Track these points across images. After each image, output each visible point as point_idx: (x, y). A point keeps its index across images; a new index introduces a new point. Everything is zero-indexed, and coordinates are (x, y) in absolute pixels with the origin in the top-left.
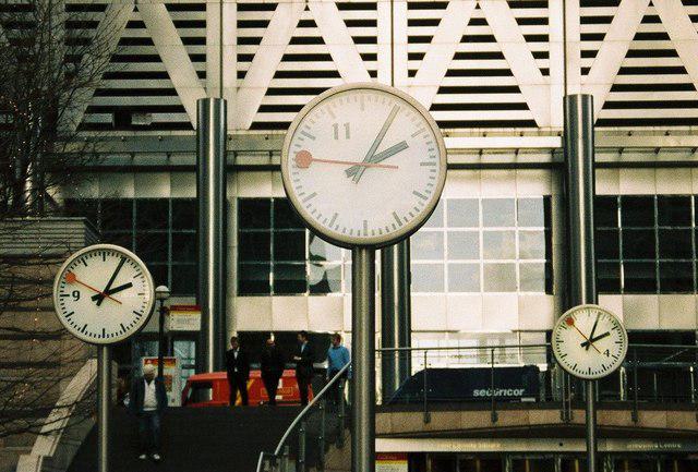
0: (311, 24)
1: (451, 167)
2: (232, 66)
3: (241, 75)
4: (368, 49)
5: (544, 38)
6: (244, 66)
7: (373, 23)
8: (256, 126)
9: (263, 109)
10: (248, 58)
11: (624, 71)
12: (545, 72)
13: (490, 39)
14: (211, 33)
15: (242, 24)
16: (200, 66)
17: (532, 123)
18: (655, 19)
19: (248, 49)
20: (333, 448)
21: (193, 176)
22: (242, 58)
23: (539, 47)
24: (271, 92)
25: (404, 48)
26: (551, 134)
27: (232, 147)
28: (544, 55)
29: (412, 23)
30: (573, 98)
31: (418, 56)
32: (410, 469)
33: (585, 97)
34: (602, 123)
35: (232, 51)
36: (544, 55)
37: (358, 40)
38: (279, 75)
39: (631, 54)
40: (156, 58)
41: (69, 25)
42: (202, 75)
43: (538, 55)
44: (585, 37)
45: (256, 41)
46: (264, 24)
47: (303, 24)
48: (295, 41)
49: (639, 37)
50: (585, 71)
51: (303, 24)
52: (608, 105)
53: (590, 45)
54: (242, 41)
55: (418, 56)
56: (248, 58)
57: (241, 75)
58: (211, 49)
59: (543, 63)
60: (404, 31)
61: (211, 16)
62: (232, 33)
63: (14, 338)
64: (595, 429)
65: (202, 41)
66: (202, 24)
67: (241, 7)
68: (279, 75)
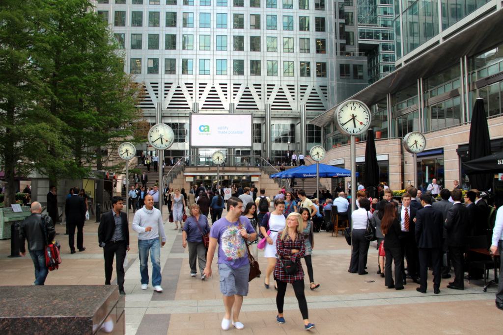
0: (214, 88)
1: (254, 117)
2: (163, 96)
3: (165, 97)
4: (156, 92)
5: (226, 91)
7: (226, 88)
8: (168, 108)
9: (170, 104)
10: (167, 94)
11: (242, 98)
12: (294, 99)
13: (283, 92)
14: (159, 89)
16: (157, 95)
17: (223, 108)
18: (248, 88)
19: (166, 92)
20: (179, 174)
21: (189, 118)
22: (165, 94)
23: (225, 93)
24: (171, 101)
25: (198, 93)
26: (261, 111)
27: (163, 112)
28: (226, 95)
29: (200, 87)
30: (231, 104)
31: (235, 95)
32: (502, 173)
33: (233, 104)
34: (237, 108)
35: (164, 92)
36: (226, 95)
37: (189, 91)
38: (173, 97)
39: (243, 95)
42: (157, 97)
43: (225, 95)
44: (234, 91)
46: (170, 87)
47: (212, 88)
48: (176, 91)
50: (234, 98)
51: (212, 88)
52: (238, 105)
53: (302, 94)
54: (268, 92)
55: (235, 95)
56: (167, 94)
57: (165, 97)
58: (159, 92)
59: (260, 97)
60: (198, 89)
65: (157, 90)
68: (173, 97)
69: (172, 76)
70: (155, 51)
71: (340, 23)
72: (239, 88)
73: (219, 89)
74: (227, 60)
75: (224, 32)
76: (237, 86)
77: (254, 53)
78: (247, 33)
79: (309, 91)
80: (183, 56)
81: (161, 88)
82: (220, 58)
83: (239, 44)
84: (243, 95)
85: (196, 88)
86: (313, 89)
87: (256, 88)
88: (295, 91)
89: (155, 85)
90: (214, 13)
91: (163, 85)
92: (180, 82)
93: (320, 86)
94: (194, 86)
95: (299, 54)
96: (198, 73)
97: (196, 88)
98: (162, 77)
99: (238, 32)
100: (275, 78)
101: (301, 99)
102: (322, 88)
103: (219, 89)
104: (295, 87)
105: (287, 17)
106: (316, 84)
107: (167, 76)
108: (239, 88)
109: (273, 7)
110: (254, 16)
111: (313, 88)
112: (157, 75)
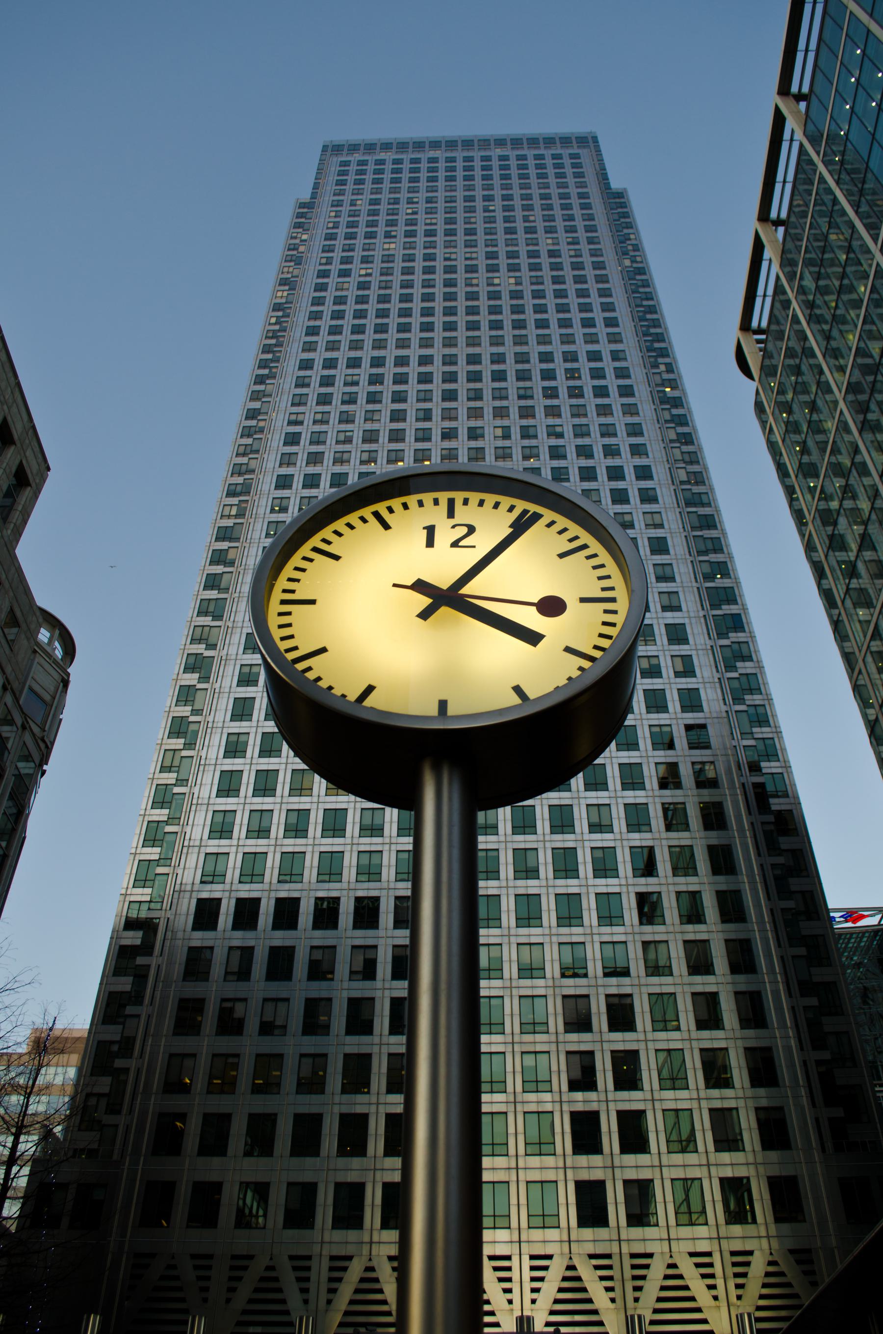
2: (324, 1296)
3: (329, 1302)
4: (507, 1285)
6: (637, 1294)
11: (556, 1301)
14: (313, 1275)
15: (532, 1268)
16: (305, 1296)
19: (639, 1283)
35: (324, 1287)
37: (501, 1280)
40: (280, 1290)
41: (196, 1267)
45: (643, 1278)
49: (565, 1279)
53: (536, 1285)
54: (533, 1279)
58: (312, 1286)
61: (314, 1264)
62: (325, 1274)
63: (633, 783)
64: (876, 271)
66: (509, 1269)
67: (532, 1257)
69: (352, 1235)
70: (309, 1161)
71: (819, 1063)
72: (546, 1268)
73: (687, 1267)
74: (508, 1182)
75: (545, 1100)
76: (540, 1262)
77: (630, 1159)
78: (608, 1102)
79: (758, 1266)
80: (743, 1161)
81: (321, 1271)
82: (536, 1176)
83: (586, 1133)
84: (561, 1290)
85: (520, 1270)
86: (770, 1263)
87: (597, 1267)
88: (718, 1269)
89: (302, 1264)
90: (692, 1048)
91: (326, 1264)
92: (374, 1253)
93: (791, 1251)
94: (515, 1263)
95: (714, 1157)
96: (524, 1224)
97: (520, 1270)
98: (325, 1237)
99: (581, 1101)
100: (650, 1232)
101: (739, 1297)
102: (595, 1262)
103: (687, 1267)
104: (716, 1259)
105: (665, 1053)
106: (775, 1244)
107: (339, 1235)
108: (546, 1268)
109: (537, 1029)
110: (577, 1057)
111: (771, 1258)
112: (307, 1232)
